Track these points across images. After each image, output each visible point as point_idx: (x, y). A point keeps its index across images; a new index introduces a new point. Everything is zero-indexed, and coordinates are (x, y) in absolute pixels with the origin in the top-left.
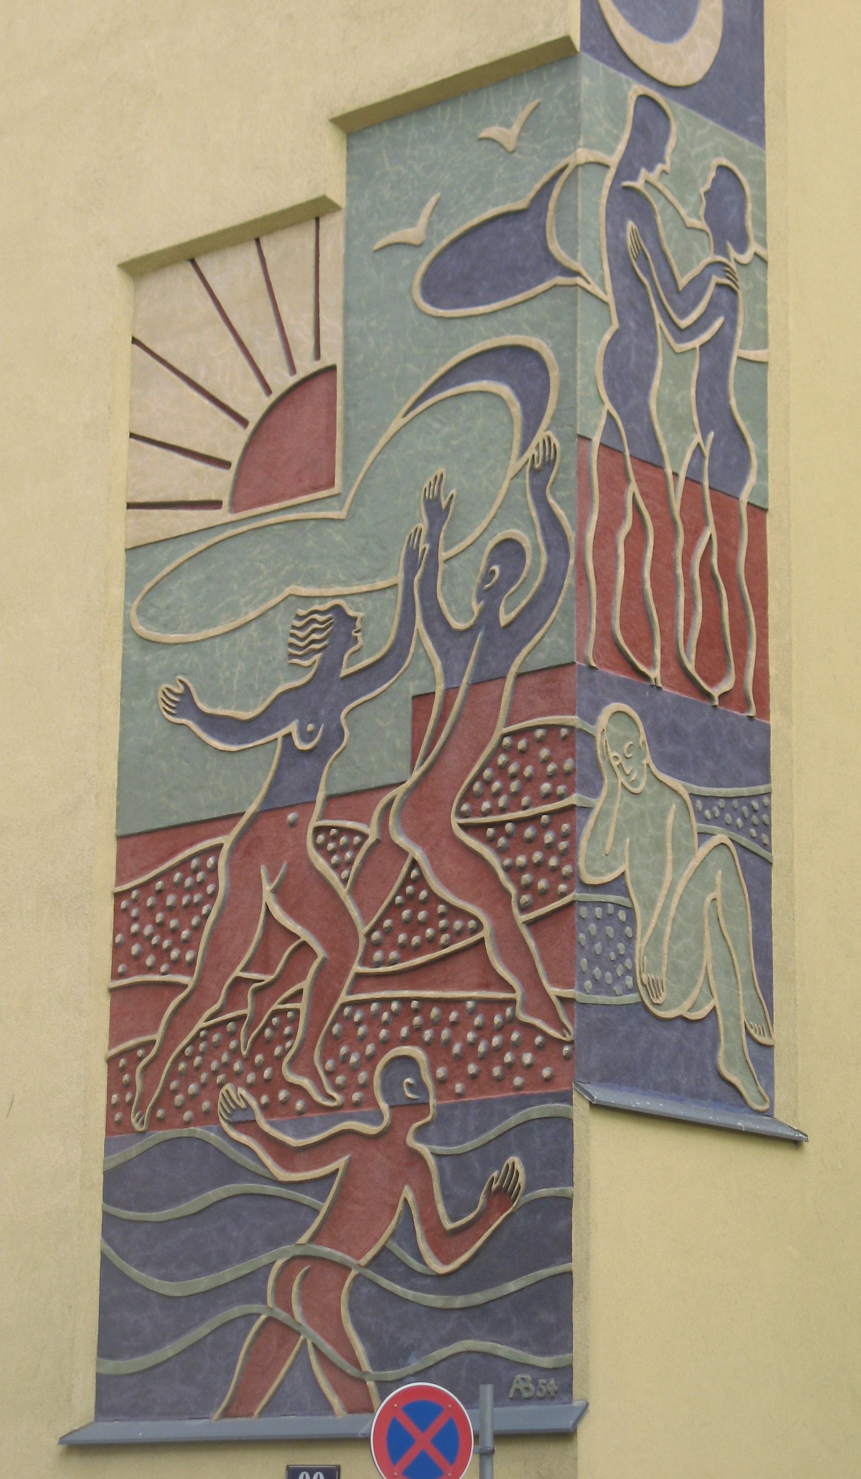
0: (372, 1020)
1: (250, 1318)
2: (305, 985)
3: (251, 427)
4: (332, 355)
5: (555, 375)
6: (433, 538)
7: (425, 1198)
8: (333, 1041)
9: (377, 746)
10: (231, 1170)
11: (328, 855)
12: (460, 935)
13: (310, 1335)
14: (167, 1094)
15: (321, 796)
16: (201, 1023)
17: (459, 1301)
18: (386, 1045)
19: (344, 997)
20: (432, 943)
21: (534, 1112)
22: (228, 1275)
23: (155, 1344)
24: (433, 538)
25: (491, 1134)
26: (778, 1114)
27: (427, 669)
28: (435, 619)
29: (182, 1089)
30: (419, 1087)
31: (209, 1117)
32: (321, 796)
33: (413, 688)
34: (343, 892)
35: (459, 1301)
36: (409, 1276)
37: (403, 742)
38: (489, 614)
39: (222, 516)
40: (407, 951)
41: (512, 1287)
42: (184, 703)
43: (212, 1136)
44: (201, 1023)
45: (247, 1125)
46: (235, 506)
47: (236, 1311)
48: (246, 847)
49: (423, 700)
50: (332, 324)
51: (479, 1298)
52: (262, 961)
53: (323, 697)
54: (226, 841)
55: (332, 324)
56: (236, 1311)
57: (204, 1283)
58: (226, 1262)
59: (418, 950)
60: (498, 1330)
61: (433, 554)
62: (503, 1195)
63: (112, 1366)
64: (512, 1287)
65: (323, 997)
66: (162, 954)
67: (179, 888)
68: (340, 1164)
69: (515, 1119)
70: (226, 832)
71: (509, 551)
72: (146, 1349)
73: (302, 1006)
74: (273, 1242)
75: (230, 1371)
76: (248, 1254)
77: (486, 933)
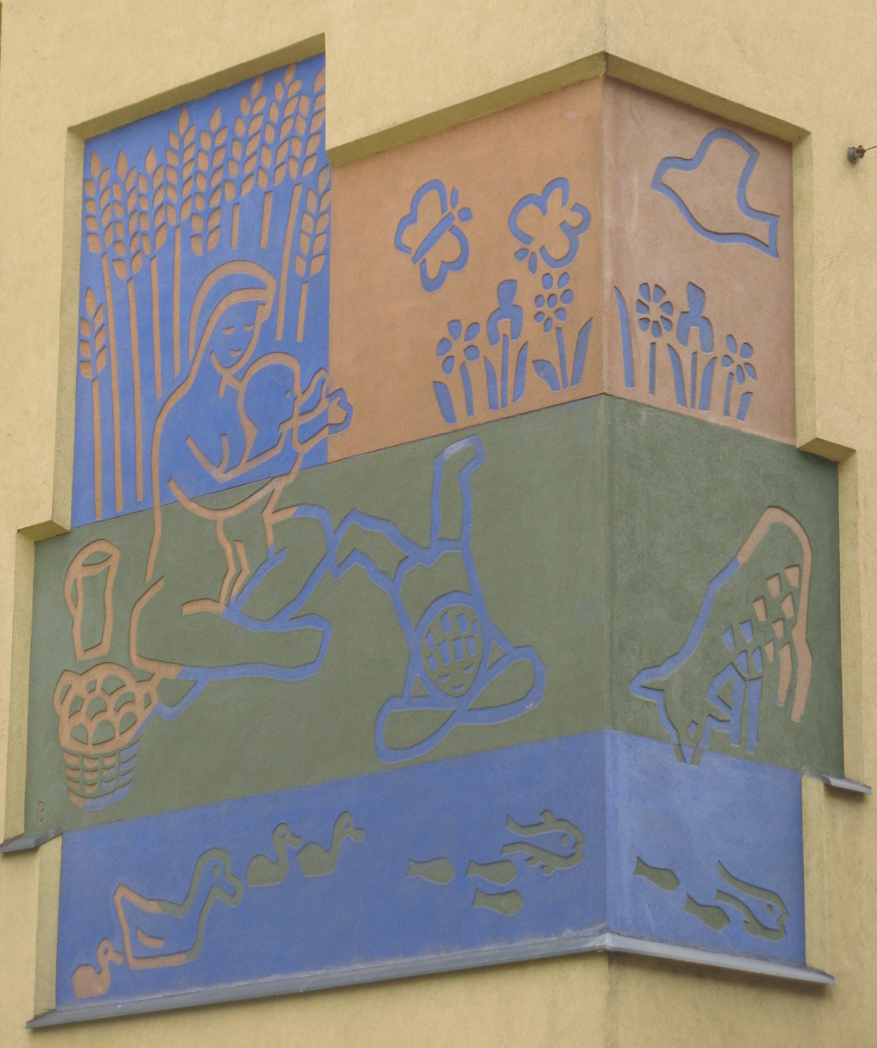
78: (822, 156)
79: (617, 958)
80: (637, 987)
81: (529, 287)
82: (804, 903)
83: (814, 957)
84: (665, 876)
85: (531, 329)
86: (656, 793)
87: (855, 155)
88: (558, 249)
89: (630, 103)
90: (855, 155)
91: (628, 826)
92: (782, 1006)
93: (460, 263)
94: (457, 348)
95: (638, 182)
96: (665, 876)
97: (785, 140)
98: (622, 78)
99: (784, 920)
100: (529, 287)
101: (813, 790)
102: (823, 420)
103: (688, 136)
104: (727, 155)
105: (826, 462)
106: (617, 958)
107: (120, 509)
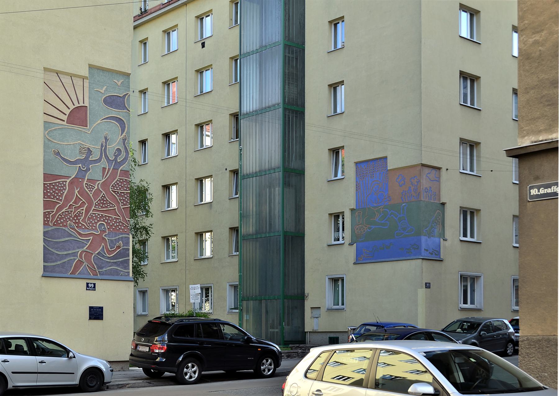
0: (96, 216)
1: (75, 259)
2: (84, 208)
3: (71, 110)
4: (86, 104)
5: (126, 126)
6: (106, 143)
7: (106, 245)
8: (89, 219)
9: (95, 172)
10: (71, 235)
11: (88, 188)
12: (111, 207)
13: (85, 263)
14: (57, 221)
15: (86, 178)
16: (64, 210)
17: (112, 261)
18: (98, 221)
19: (91, 212)
20: (106, 207)
21: (124, 236)
22: (70, 252)
23: (56, 261)
24: (106, 143)
25: (117, 237)
26: (277, 102)
27: (104, 163)
28: (106, 156)
29: (60, 220)
30: (105, 228)
31: (66, 226)
32: (86, 178)
33: (103, 166)
34: (91, 195)
35: (112, 261)
36: (103, 256)
37: (101, 174)
38: (115, 160)
39: (65, 123)
40: (102, 207)
41: (120, 260)
42: (58, 154)
43: (66, 229)
44: (64, 210)
45: (73, 229)
46: (67, 123)
47: (72, 258)
48: (71, 183)
49: (104, 169)
50: (86, 99)
51: (115, 261)
52: (75, 202)
53: (86, 161)
54: (68, 181)
55: (86, 99)
56: (72, 258)
57: (65, 253)
58: (69, 250)
59: (104, 208)
60: (118, 266)
61: (106, 146)
62: (119, 247)
63: (46, 264)
64: (120, 260)
65: (87, 211)
66: (55, 197)
67: (58, 186)
68: (91, 238)
69: (121, 236)
70: (68, 179)
71: (118, 150)
72: (54, 262)
73: (84, 212)
74: (78, 248)
75: (71, 267)
76: (74, 249)
77: (85, 182)
78: (444, 170)
79: (423, 259)
80: (425, 261)
81: (412, 188)
82: (519, 192)
83: (442, 257)
84: (427, 250)
85: (413, 192)
86: (425, 241)
87: (447, 169)
88: (416, 184)
89: (424, 168)
90: (447, 169)
91: (424, 246)
92: (438, 262)
93: (404, 184)
94: (404, 194)
95: (424, 176)
96: (427, 250)
97: (439, 169)
98: (423, 165)
99: (438, 253)
100: (412, 188)
101: (442, 240)
102: (443, 201)
103: (430, 169)
104: (434, 171)
105: (443, 204)
106: (423, 259)
107: (171, 103)
